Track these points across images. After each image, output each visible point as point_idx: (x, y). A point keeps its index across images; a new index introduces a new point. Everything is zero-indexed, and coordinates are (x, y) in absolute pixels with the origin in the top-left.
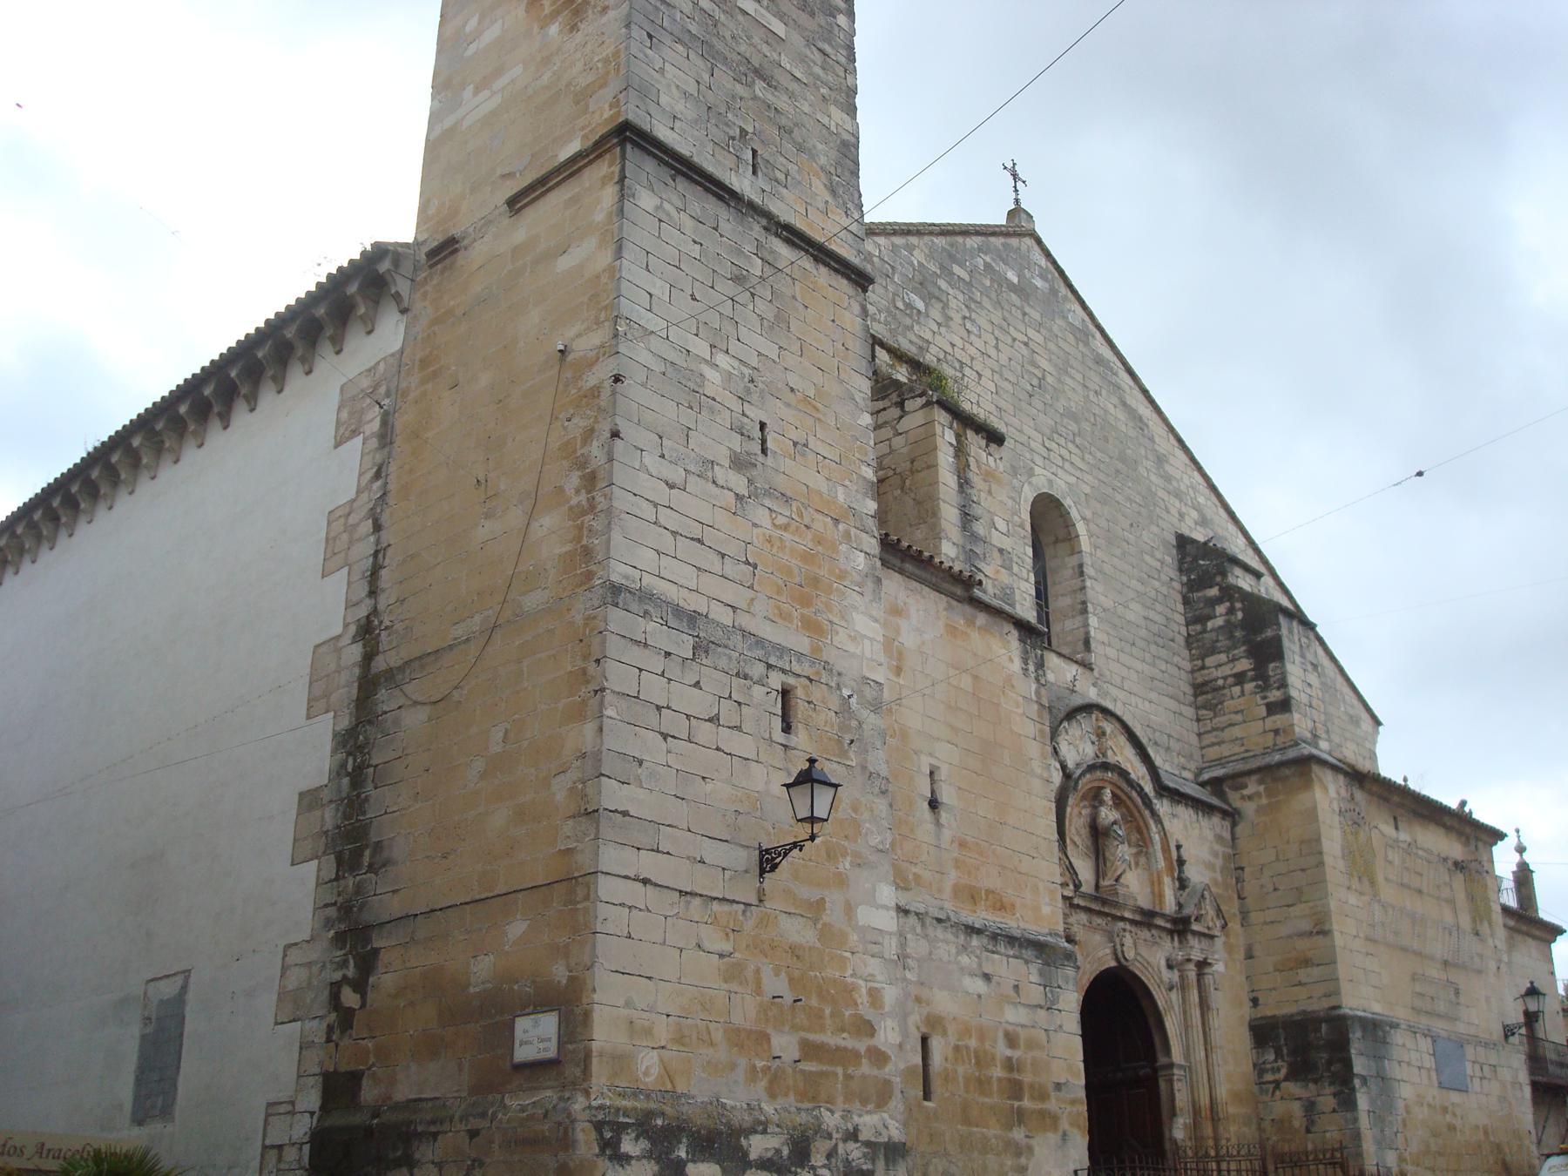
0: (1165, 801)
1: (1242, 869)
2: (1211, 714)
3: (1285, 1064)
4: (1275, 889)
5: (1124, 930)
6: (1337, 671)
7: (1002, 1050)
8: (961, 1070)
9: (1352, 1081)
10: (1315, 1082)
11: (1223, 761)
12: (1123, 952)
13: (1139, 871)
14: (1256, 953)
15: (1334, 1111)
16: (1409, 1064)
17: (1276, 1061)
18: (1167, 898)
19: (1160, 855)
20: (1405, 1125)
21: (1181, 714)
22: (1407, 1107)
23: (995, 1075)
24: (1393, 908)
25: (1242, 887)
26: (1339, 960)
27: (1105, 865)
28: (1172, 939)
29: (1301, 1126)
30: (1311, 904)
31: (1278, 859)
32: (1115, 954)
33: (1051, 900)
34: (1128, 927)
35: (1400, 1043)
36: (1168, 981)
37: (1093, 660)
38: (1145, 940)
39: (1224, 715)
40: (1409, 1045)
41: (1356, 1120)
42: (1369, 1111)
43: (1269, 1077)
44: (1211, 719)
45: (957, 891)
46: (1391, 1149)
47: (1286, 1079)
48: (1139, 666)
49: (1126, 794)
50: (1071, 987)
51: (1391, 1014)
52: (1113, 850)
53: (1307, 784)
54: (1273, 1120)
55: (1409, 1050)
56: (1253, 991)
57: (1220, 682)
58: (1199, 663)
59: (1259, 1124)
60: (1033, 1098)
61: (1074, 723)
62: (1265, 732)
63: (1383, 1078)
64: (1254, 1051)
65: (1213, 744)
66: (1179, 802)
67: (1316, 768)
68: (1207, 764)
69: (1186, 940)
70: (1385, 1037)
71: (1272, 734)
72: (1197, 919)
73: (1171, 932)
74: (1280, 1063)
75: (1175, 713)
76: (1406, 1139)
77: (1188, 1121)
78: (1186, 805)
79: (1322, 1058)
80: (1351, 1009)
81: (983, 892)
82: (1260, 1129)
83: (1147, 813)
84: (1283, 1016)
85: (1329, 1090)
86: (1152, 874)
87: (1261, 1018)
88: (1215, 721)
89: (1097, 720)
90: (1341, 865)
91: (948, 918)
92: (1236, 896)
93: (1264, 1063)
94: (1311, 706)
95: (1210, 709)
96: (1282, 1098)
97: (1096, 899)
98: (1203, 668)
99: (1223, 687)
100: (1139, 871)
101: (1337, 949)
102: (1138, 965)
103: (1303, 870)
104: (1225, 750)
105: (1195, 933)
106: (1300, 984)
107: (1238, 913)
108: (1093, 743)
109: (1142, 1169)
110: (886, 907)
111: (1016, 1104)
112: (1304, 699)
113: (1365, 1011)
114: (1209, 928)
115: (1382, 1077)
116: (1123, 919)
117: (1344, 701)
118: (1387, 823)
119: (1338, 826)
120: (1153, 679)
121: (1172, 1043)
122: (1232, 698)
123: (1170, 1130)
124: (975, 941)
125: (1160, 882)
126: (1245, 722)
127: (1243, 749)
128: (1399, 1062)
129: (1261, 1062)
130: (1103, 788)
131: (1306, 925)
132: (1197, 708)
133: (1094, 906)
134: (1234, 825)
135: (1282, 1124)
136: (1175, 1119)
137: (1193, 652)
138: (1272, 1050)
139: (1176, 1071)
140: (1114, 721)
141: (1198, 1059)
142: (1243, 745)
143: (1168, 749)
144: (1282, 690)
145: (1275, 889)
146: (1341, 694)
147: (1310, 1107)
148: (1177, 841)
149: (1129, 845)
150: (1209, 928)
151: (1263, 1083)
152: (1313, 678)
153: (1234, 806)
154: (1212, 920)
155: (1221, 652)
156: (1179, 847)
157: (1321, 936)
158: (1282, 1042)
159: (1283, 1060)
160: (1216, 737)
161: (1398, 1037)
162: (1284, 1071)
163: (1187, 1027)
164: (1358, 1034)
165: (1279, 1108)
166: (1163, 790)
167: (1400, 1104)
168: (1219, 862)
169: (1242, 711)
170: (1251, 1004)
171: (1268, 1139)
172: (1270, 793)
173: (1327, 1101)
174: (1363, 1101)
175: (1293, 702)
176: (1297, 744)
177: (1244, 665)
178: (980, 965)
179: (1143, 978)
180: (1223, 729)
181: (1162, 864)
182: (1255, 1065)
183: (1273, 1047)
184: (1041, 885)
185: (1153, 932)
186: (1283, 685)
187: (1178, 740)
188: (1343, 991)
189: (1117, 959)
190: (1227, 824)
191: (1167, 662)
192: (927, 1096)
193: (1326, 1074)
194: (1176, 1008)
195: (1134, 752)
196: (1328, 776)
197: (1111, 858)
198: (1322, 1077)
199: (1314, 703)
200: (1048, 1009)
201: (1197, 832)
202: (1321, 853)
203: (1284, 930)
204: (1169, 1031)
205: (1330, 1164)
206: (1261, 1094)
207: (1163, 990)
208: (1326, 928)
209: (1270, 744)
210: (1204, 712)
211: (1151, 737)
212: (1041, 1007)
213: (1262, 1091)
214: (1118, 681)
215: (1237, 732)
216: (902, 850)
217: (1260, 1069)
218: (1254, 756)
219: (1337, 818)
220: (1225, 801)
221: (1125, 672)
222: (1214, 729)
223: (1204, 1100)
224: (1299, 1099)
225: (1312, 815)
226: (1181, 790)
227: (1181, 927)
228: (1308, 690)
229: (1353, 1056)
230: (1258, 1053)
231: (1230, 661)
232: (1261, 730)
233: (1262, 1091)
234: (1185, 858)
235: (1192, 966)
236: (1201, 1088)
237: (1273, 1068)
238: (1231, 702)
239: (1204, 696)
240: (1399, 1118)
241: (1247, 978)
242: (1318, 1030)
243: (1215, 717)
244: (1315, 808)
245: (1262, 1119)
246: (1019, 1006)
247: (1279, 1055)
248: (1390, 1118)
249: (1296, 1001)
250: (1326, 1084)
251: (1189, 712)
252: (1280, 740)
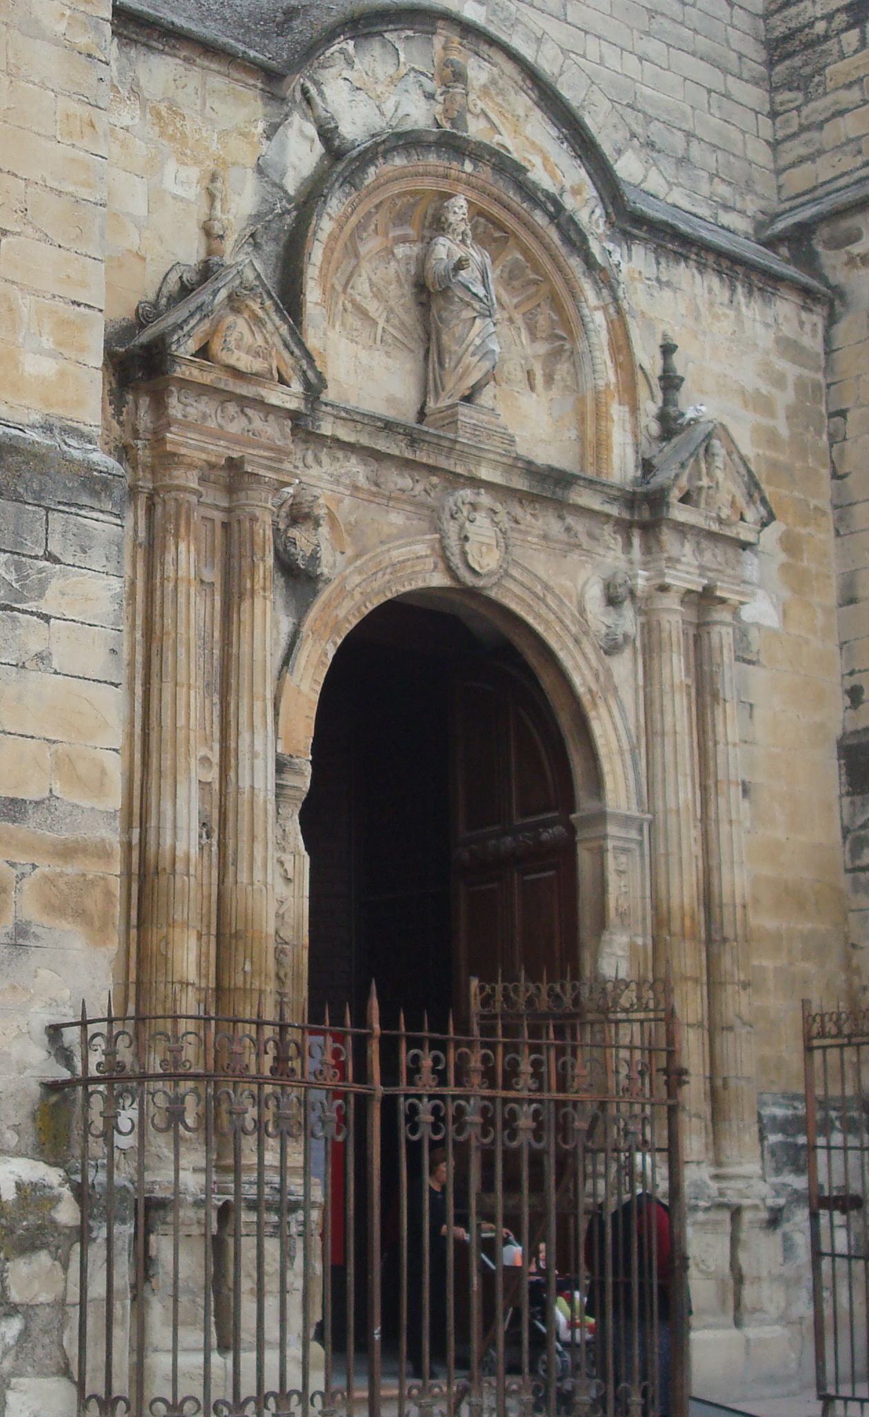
0: (638, 250)
1: (842, 413)
2: (799, 97)
5: (474, 507)
12: (464, 554)
13: (555, 392)
18: (616, 451)
19: (604, 356)
21: (727, 96)
25: (842, 453)
27: (441, 364)
28: (628, 544)
32: (443, 553)
33: (59, 344)
34: (485, 499)
36: (604, 630)
38: (545, 537)
39: (825, 94)
44: (798, 109)
49: (516, 215)
50: (96, 559)
52: (458, 330)
56: (851, 673)
57: (820, 27)
59: (848, 959)
61: (376, 46)
65: (801, 160)
66: (679, 257)
68: (787, 205)
69: (659, 542)
72: (686, 499)
73: (625, 528)
75: (709, 91)
77: (640, 941)
78: (702, 267)
86: (582, 400)
88: (806, 111)
89: (445, 48)
92: (826, 472)
95: (798, 88)
97: (413, 439)
99: (826, 37)
100: (555, 392)
104: (823, 170)
105: (682, 529)
107: (828, 508)
108: (430, 96)
109: (414, 1043)
114: (720, 521)
116: (475, 483)
122: (842, 56)
125: (600, 415)
130: (450, 196)
132: (773, 89)
133: (382, 445)
134: (832, 320)
136: (606, 936)
139: (612, 829)
140: (499, 58)
141: (672, 804)
142: (860, 152)
143: (683, 161)
148: (665, 336)
149: (533, 336)
150: (720, 521)
153: (833, 281)
156: (668, 350)
160: (806, 144)
163: (651, 731)
168: (785, 398)
169: (860, 80)
170: (848, 702)
179: (530, 620)
180: (820, 126)
181: (608, 374)
182: (846, 831)
184: (25, 304)
185: (570, 520)
187: (715, 147)
189: (451, 571)
190: (816, 319)
195: (554, 133)
197: (455, 348)
201: (727, 326)
204: (600, 742)
206: (856, 891)
207: (589, 650)
211: (638, 130)
220: (817, 273)
222: (803, 129)
226: (683, 227)
227: (646, 515)
230: (852, 803)
234: (680, 373)
235: (671, 602)
236: (674, 869)
238: (840, 65)
239: (787, 63)
241: (842, 645)
243: (807, 101)
245: (854, 946)
251: (754, 96)
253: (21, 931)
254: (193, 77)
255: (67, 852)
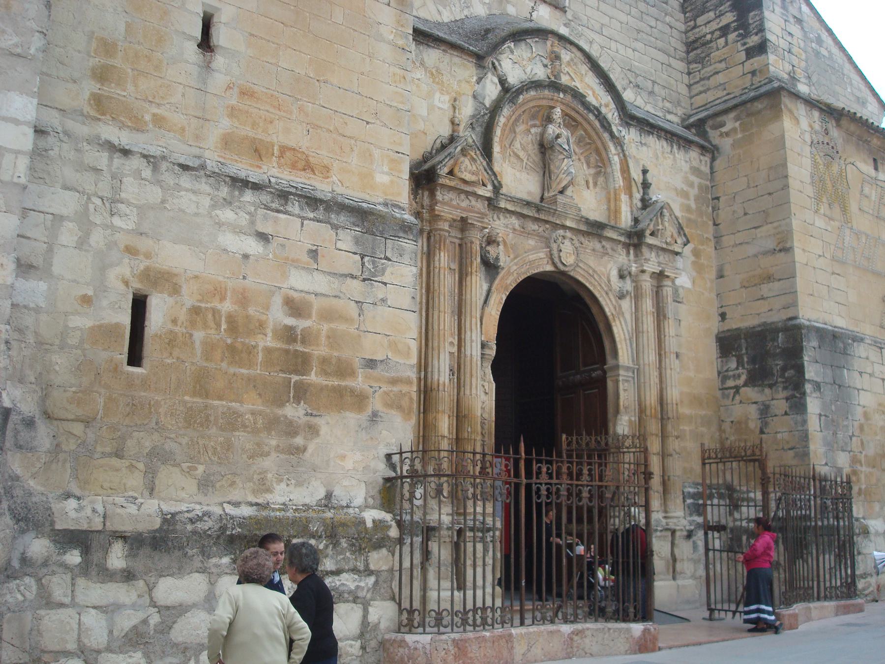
1: (718, 198)
2: (700, 66)
3: (745, 371)
4: (745, 214)
6: (845, 59)
7: (278, 316)
8: (199, 335)
9: (804, 385)
10: (771, 386)
11: (708, 106)
12: (560, 257)
13: (598, 189)
14: (726, 273)
15: (786, 414)
16: (871, 375)
17: (737, 368)
18: (623, 214)
19: (618, 174)
20: (861, 428)
21: (670, 66)
22: (866, 415)
23: (261, 345)
24: (867, 236)
25: (717, 215)
26: (798, 275)
27: (550, 178)
28: (628, 253)
29: (756, 427)
30: (775, 224)
31: (749, 187)
33: (391, 169)
34: (568, 234)
35: (863, 355)
37: (567, 4)
38: (594, 250)
39: (711, 65)
40: (873, 358)
41: (805, 422)
42: (820, 415)
43: (731, 383)
45: (227, 142)
46: (843, 451)
47: (745, 385)
48: (623, 17)
51: (855, 329)
52: (557, 164)
53: (776, 112)
54: (732, 422)
55: (873, 363)
56: (721, 307)
57: (709, 37)
58: (692, 23)
59: (720, 426)
60: (325, 373)
62: (744, 74)
63: (840, 386)
64: (719, 360)
65: (701, 93)
66: (650, 133)
67: (786, 101)
68: (695, 111)
69: (641, 252)
70: (845, 348)
71: (750, 75)
72: (652, 234)
74: (741, 370)
76: (862, 443)
77: (633, 419)
78: (659, 137)
79: (777, 365)
80: (809, 320)
81: (276, 148)
82: (721, 430)
83: (606, 135)
84: (746, 328)
85: (782, 394)
86: (609, 193)
87: (728, 330)
88: (702, 72)
90: (810, 190)
91: (203, 167)
92: (711, 223)
93: (727, 371)
94: (789, 52)
95: (699, 63)
96: (741, 402)
98: (695, 27)
99: (711, 41)
100: (598, 189)
101: (797, 265)
102: (580, 270)
103: (770, 194)
104: (710, 96)
105: (651, 247)
106: (763, 298)
107: (712, 238)
108: (545, 66)
110: (16, 122)
111: (295, 378)
112: (783, 44)
113: (826, 324)
114: (667, 243)
115: (839, 385)
116: (564, 227)
117: (851, 84)
118: (865, 162)
119: (809, 155)
120: (639, 31)
121: (619, 346)
122: (718, 49)
123: (615, 425)
124: (249, 196)
125: (617, 199)
126: (727, 68)
127: (725, 92)
128: (861, 373)
129: (725, 369)
130: (554, 107)
131: (771, 244)
132: (689, 63)
133: (525, 211)
135: (739, 425)
136: (619, 417)
137: (687, 15)
138: (734, 359)
139: (621, 372)
140: (574, 50)
141: (646, 362)
142: (725, 89)
143: (651, 93)
144: (760, 35)
145: (745, 214)
146: (849, 77)
147: (765, 411)
148: (644, 166)
150: (667, 243)
151: (726, 389)
152: (795, 29)
153: (714, 143)
154: (672, 236)
155: (710, 10)
156: (645, 172)
157: (782, 254)
158: (744, 351)
159: (744, 368)
161: (861, 350)
162: (744, 378)
163: (638, 331)
164: (815, 343)
165: (738, 411)
166: (629, 118)
167: (859, 412)
168: (693, 192)
170: (720, 319)
171: (727, 439)
172: (744, 128)
173: (780, 405)
174: (813, 405)
175: (768, 44)
176: (771, 81)
177: (729, 18)
178: (252, 223)
179: (587, 285)
180: (708, 78)
181: (620, 182)
182: (719, 373)
183: (735, 356)
184: (377, 153)
185: (604, 243)
186: (761, 30)
187: (664, 87)
188: (800, 303)
189: (554, 264)
190: (707, 159)
191: (657, 20)
192: (135, 357)
193: (780, 380)
194: (628, 316)
196: (801, 110)
198: (776, 382)
199: (795, 50)
200: (364, 280)
201: (669, 162)
202: (786, 177)
203: (751, 250)
204: (616, 336)
205: (750, 461)
206: (723, 398)
208: (788, 245)
209: (748, 85)
210: (695, 65)
211: (633, 80)
212: (353, 277)
213: (724, 396)
214: (597, 27)
215: (720, 78)
216: (136, 86)
217: (723, 376)
218: (734, 97)
219: (807, 149)
221: (606, 20)
222: (702, 79)
223: (651, 398)
224: (755, 403)
225: (780, 143)
226: (651, 120)
227: (636, 241)
228: (789, 39)
229: (806, 363)
231: (716, 17)
232: (741, 74)
233: (724, 396)
234: (650, 181)
235: (646, 277)
237: (734, 376)
238: (717, 53)
239: (695, 52)
240: (856, 424)
241: (718, 295)
242: (775, 339)
243: (703, 68)
244: (783, 136)
245: (723, 421)
246: (315, 273)
247: (740, 363)
248: (845, 423)
249: (759, 314)
250: (780, 389)
251: (681, 66)
252: (757, 79)
253: (375, 414)
254: (447, 58)
255: (394, 381)
